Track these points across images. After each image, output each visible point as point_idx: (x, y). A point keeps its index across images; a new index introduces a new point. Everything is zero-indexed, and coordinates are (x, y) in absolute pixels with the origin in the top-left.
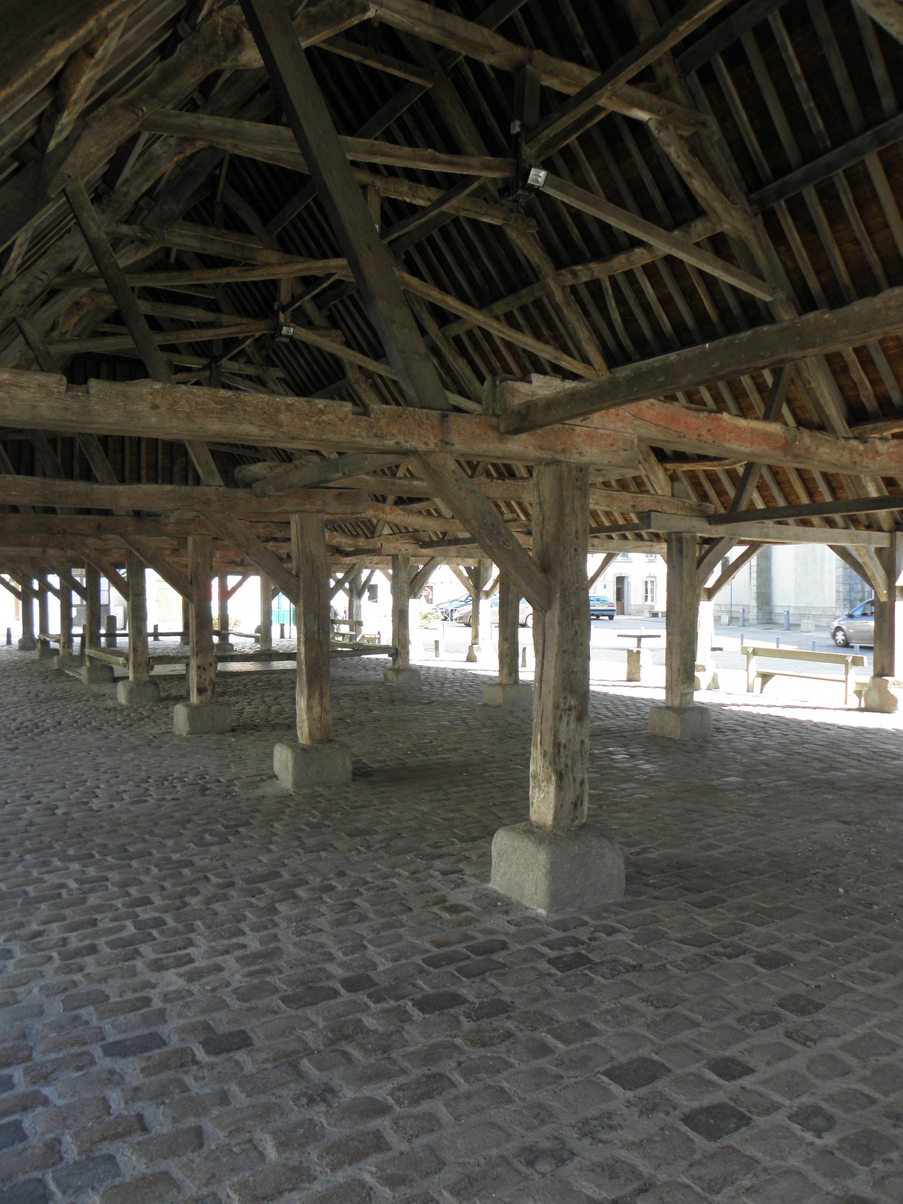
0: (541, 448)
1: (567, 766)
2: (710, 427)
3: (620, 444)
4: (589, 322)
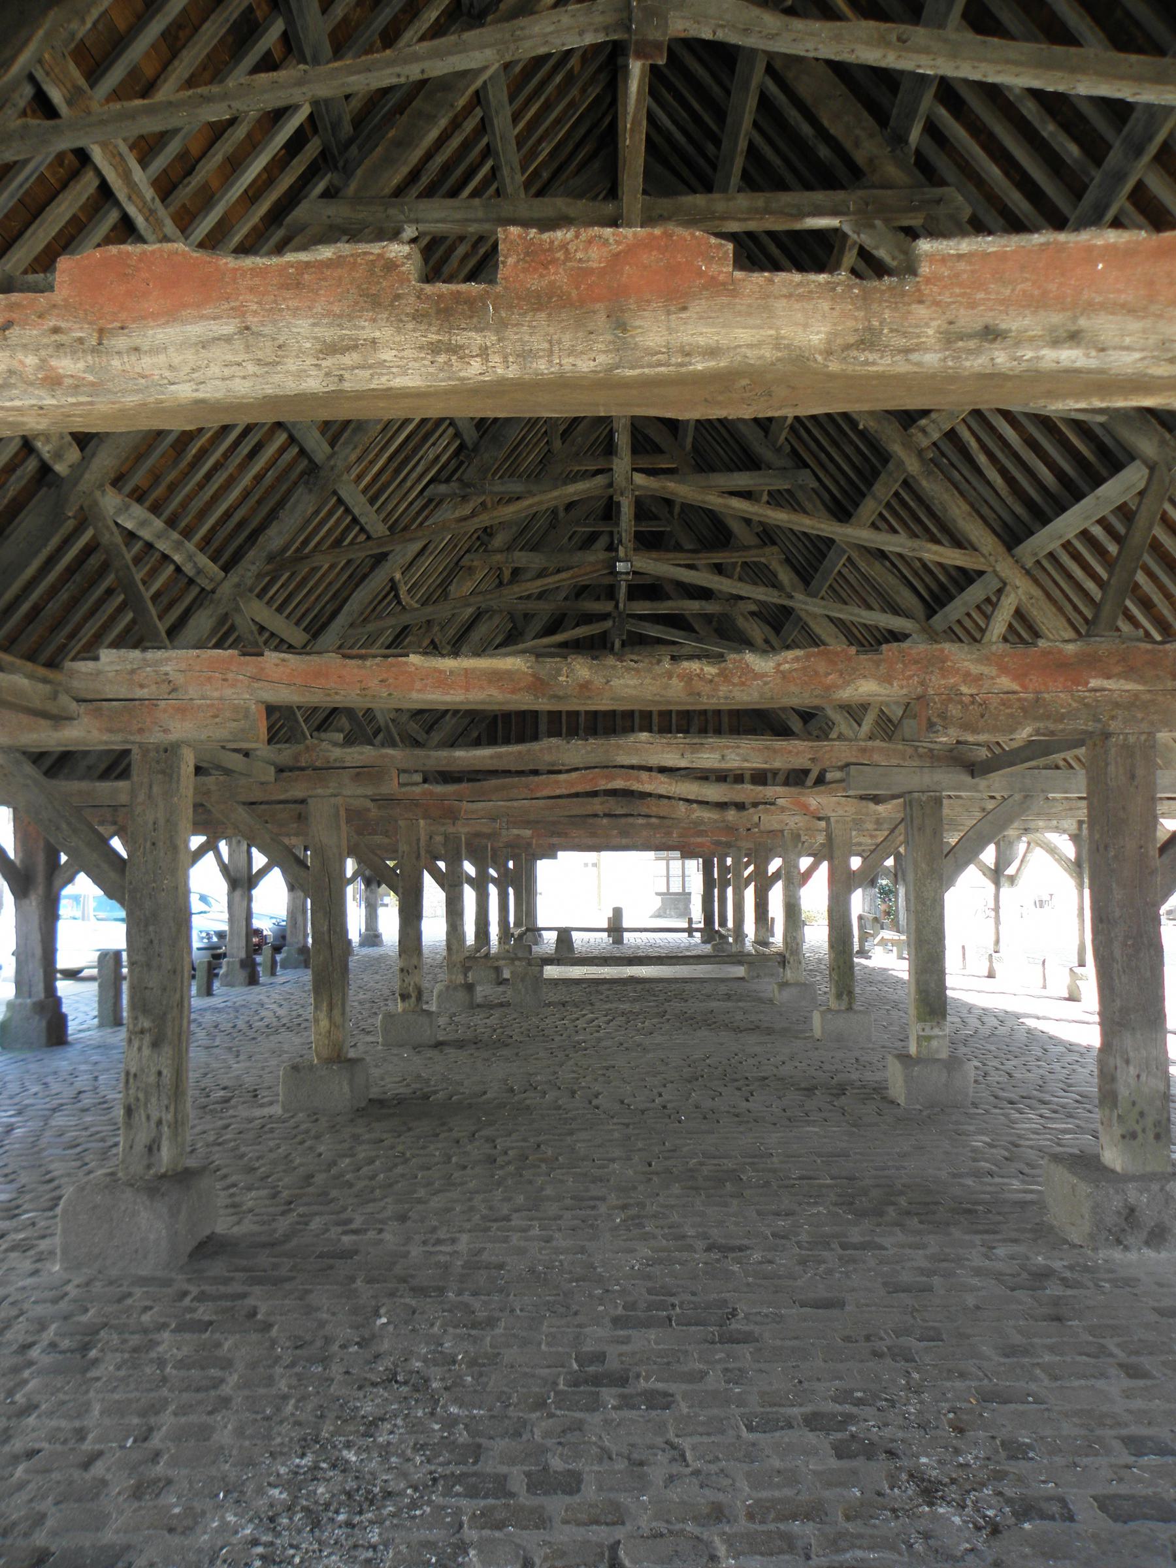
0: (110, 731)
1: (138, 1099)
2: (385, 676)
3: (228, 714)
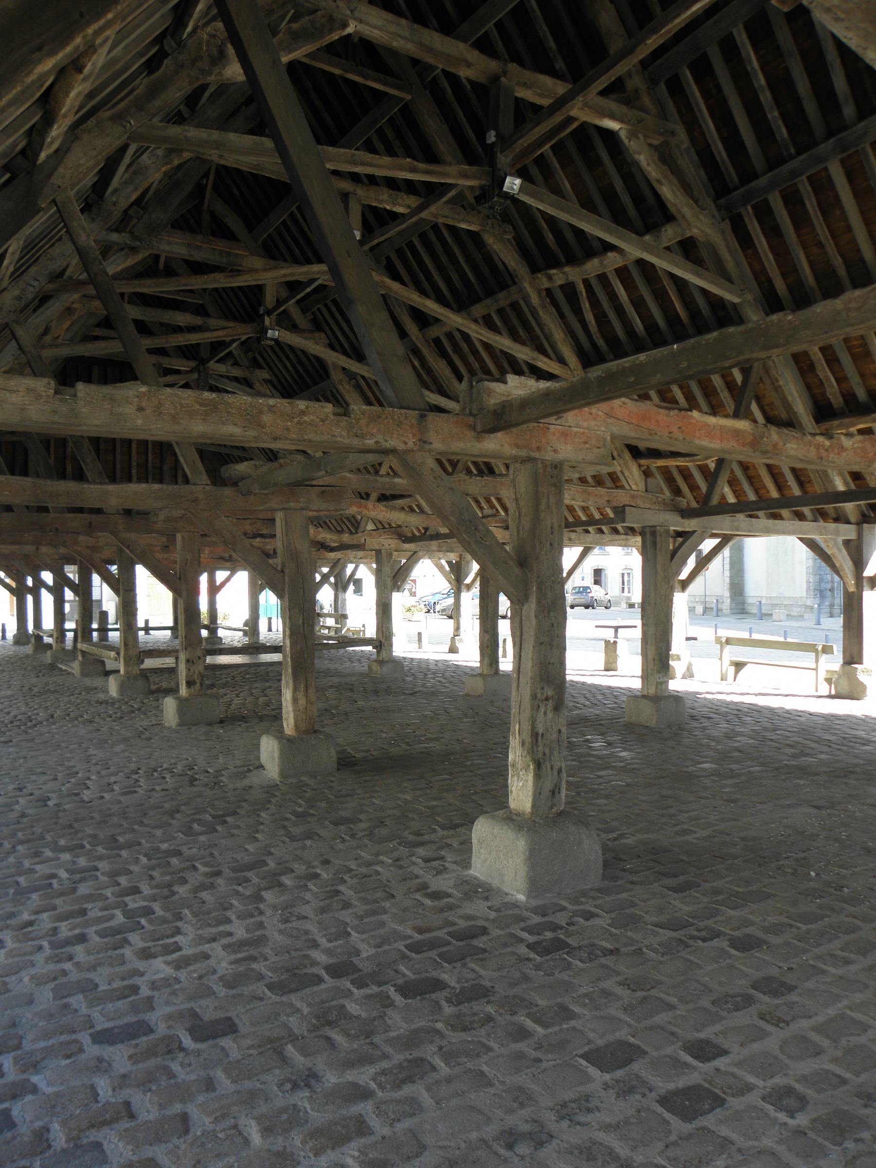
0: (517, 446)
1: (544, 754)
3: (594, 442)
4: (565, 323)
